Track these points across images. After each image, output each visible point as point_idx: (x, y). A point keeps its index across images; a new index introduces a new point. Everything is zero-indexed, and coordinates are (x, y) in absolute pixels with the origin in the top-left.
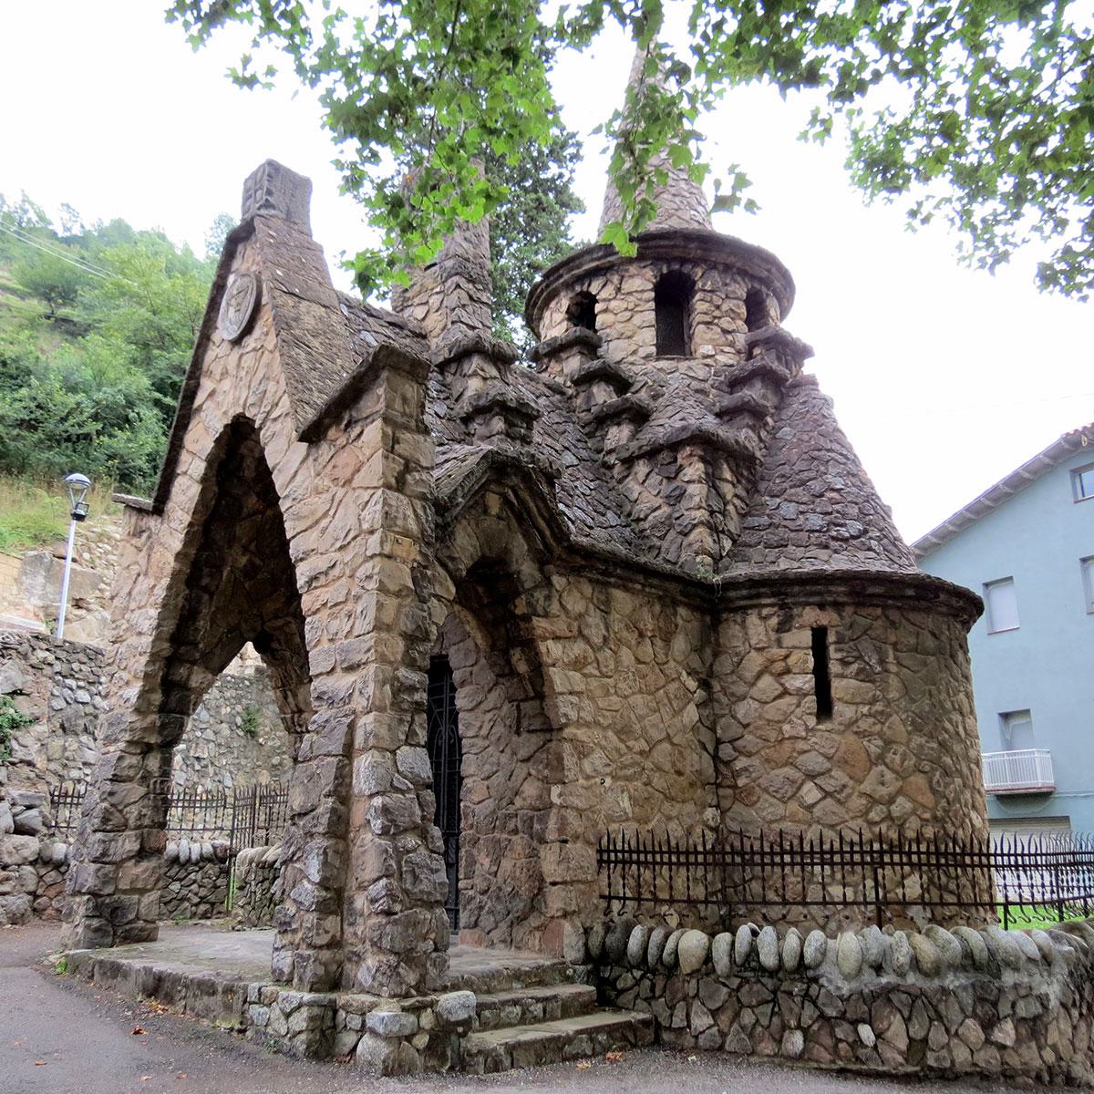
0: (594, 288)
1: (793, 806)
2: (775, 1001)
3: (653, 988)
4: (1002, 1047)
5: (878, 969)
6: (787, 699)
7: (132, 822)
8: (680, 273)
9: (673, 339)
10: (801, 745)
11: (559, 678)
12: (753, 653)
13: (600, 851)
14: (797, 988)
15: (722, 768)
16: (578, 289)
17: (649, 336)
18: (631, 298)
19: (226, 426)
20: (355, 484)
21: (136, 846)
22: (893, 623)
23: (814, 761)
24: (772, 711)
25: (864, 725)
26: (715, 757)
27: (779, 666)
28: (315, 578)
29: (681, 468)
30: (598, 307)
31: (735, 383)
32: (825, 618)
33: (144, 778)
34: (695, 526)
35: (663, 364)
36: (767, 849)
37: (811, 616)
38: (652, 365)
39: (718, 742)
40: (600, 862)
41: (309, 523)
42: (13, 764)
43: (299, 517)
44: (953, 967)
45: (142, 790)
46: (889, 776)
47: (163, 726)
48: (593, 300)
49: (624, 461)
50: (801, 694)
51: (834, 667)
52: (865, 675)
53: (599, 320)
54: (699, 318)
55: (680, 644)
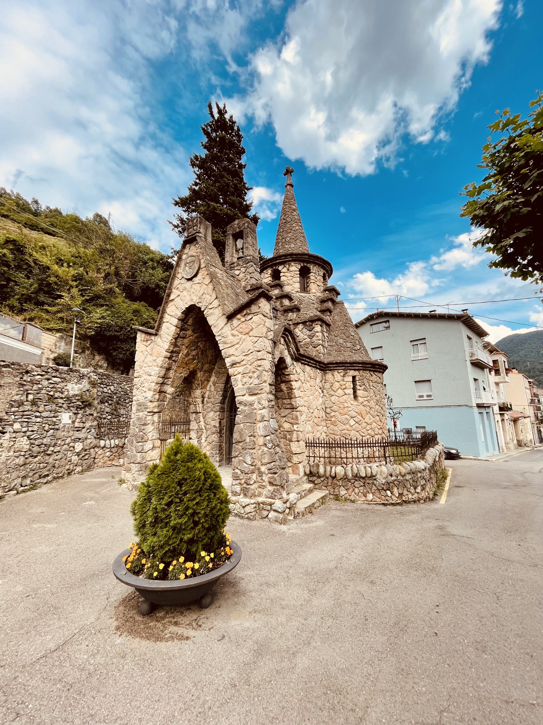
0: (280, 268)
1: (347, 426)
2: (364, 486)
3: (327, 483)
4: (418, 493)
5: (391, 475)
6: (346, 396)
7: (150, 439)
8: (306, 266)
9: (304, 288)
10: (350, 409)
11: (296, 393)
12: (336, 383)
13: (306, 443)
14: (371, 482)
15: (327, 415)
16: (274, 268)
17: (297, 285)
18: (291, 273)
19: (186, 308)
20: (251, 334)
21: (152, 446)
22: (371, 375)
23: (353, 414)
24: (341, 399)
25: (366, 403)
26: (326, 412)
27: (344, 387)
28: (235, 364)
29: (314, 328)
30: (281, 274)
31: (323, 301)
32: (356, 373)
33: (153, 423)
34: (319, 345)
35: (302, 294)
36: (353, 443)
37: (352, 373)
38: (298, 294)
39: (326, 408)
40: (306, 446)
41: (230, 345)
42: (87, 415)
43: (225, 343)
44: (409, 473)
45: (153, 428)
46: (371, 417)
47: (159, 406)
48: (280, 272)
49: (294, 324)
50: (349, 394)
51: (358, 387)
52: (365, 390)
53: (282, 279)
54: (312, 281)
55: (318, 380)
